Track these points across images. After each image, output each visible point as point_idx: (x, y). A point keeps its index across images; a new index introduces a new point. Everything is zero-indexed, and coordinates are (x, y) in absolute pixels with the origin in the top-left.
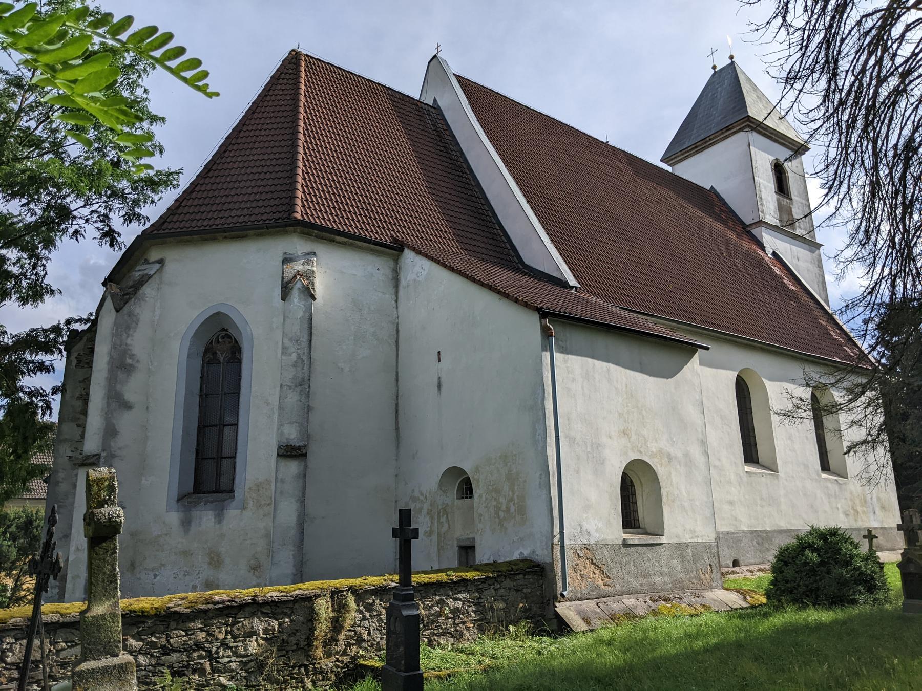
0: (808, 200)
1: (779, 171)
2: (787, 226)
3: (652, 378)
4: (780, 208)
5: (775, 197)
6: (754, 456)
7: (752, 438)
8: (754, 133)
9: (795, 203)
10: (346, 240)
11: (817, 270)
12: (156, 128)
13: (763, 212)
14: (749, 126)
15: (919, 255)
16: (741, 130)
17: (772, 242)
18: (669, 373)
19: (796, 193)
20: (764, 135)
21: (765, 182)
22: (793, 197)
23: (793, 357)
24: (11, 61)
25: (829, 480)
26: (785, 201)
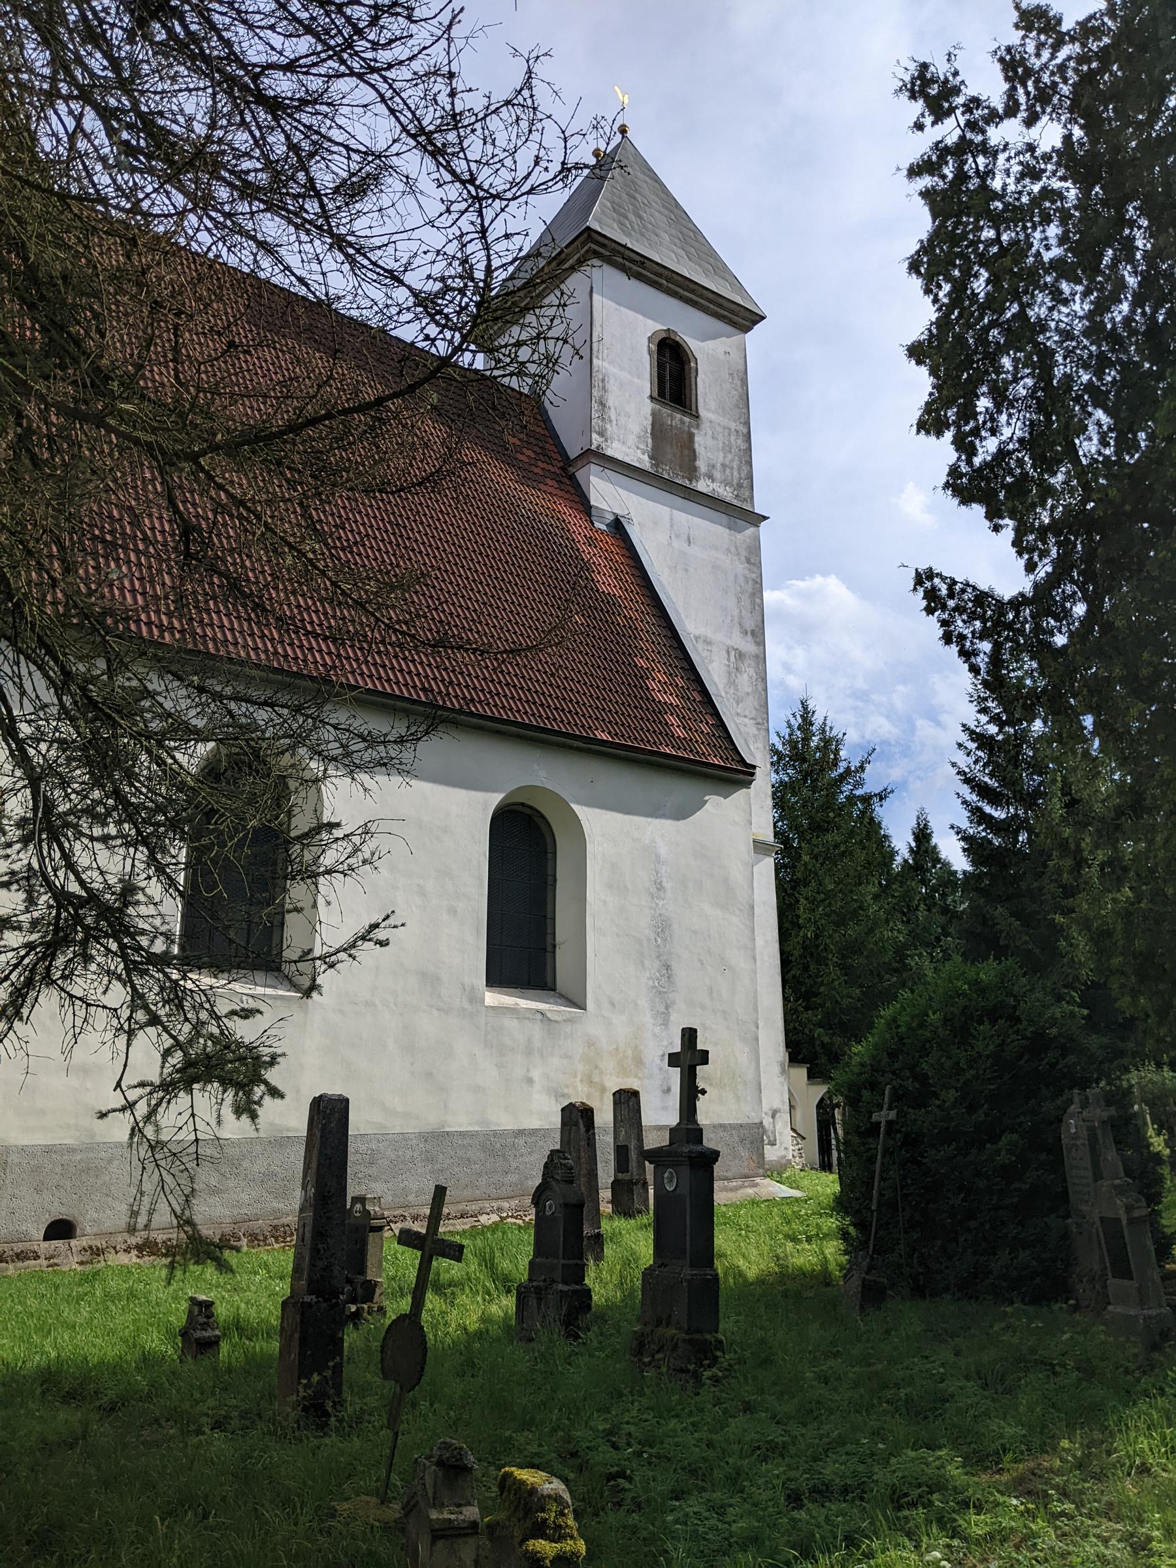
0: (747, 424)
1: (673, 371)
2: (671, 470)
3: (627, 817)
4: (658, 431)
5: (648, 407)
6: (549, 980)
7: (549, 938)
8: (607, 269)
9: (705, 425)
10: (581, 745)
11: (741, 568)
12: (964, 824)
13: (601, 434)
14: (598, 255)
15: (735, 1562)
16: (581, 262)
17: (606, 494)
18: (682, 813)
19: (713, 405)
20: (639, 277)
21: (624, 375)
22: (702, 412)
23: (564, 746)
24: (3, 538)
25: (513, 1011)
26: (677, 419)
